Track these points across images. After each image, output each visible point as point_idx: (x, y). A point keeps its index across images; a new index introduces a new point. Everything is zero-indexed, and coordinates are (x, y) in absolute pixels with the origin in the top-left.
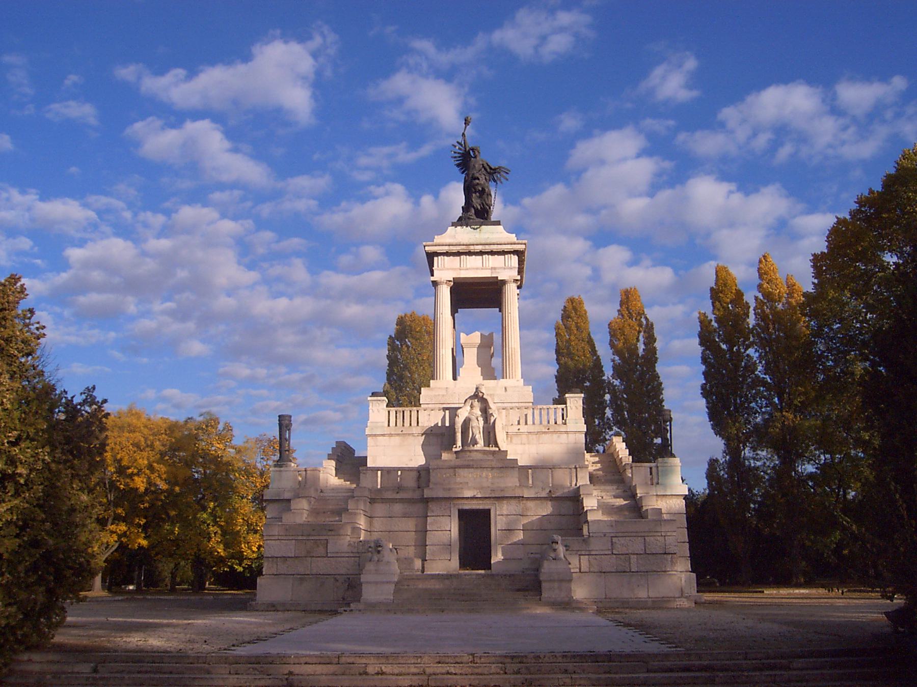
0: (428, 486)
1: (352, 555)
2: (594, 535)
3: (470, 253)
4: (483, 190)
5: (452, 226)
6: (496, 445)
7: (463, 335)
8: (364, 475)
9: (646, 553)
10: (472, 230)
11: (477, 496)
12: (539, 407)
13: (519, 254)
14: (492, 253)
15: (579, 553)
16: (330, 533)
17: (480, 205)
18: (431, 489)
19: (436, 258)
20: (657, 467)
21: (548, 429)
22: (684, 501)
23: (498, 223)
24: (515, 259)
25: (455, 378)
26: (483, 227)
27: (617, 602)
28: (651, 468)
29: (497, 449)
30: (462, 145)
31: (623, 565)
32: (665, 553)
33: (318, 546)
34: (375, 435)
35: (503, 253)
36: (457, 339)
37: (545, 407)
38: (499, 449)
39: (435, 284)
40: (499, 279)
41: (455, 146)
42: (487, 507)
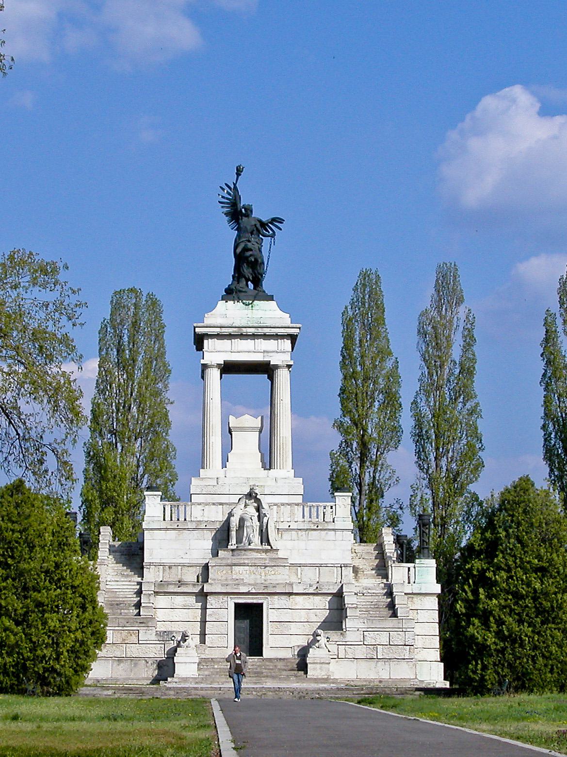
0: (208, 582)
1: (158, 642)
2: (350, 629)
3: (242, 336)
4: (256, 260)
5: (222, 300)
6: (269, 544)
7: (232, 418)
8: (148, 570)
9: (364, 644)
10: (244, 306)
11: (251, 591)
12: (309, 504)
13: (293, 338)
14: (265, 337)
15: (338, 643)
16: (141, 625)
17: (252, 274)
18: (211, 584)
19: (205, 342)
20: (415, 568)
21: (317, 527)
22: (437, 599)
23: (271, 298)
24: (287, 343)
25: (224, 466)
26: (256, 302)
27: (366, 681)
28: (409, 568)
29: (269, 548)
30: (230, 188)
31: (372, 653)
32: (405, 645)
33: (131, 635)
34: (152, 529)
35: (277, 337)
36: (225, 421)
37: (314, 504)
38: (271, 548)
39: (205, 367)
40: (271, 363)
41: (223, 189)
42: (260, 601)
